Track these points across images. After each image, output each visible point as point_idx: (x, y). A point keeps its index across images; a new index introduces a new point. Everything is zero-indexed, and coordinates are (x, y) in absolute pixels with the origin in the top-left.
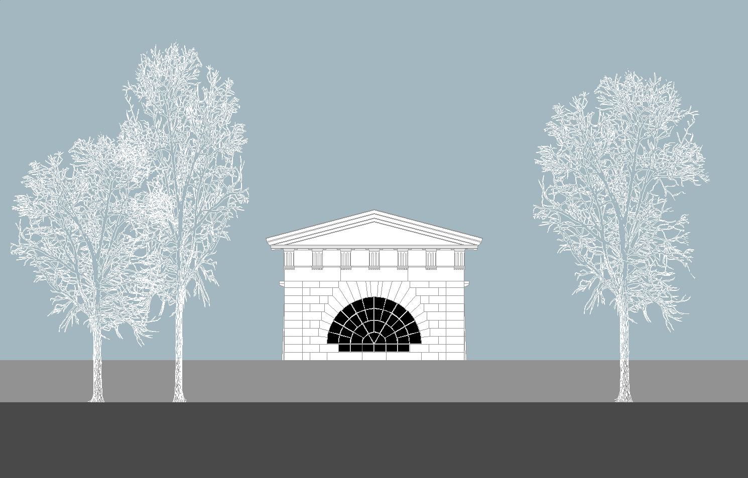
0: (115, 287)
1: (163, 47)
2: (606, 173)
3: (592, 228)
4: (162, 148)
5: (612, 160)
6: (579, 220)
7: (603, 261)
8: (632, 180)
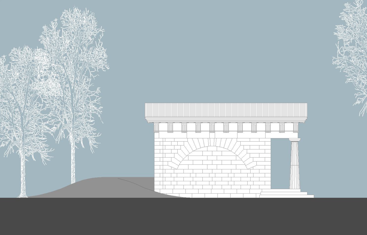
0: (32, 132)
2: (14, 92)
3: (8, 117)
5: (17, 87)
6: (357, 65)
7: (13, 133)
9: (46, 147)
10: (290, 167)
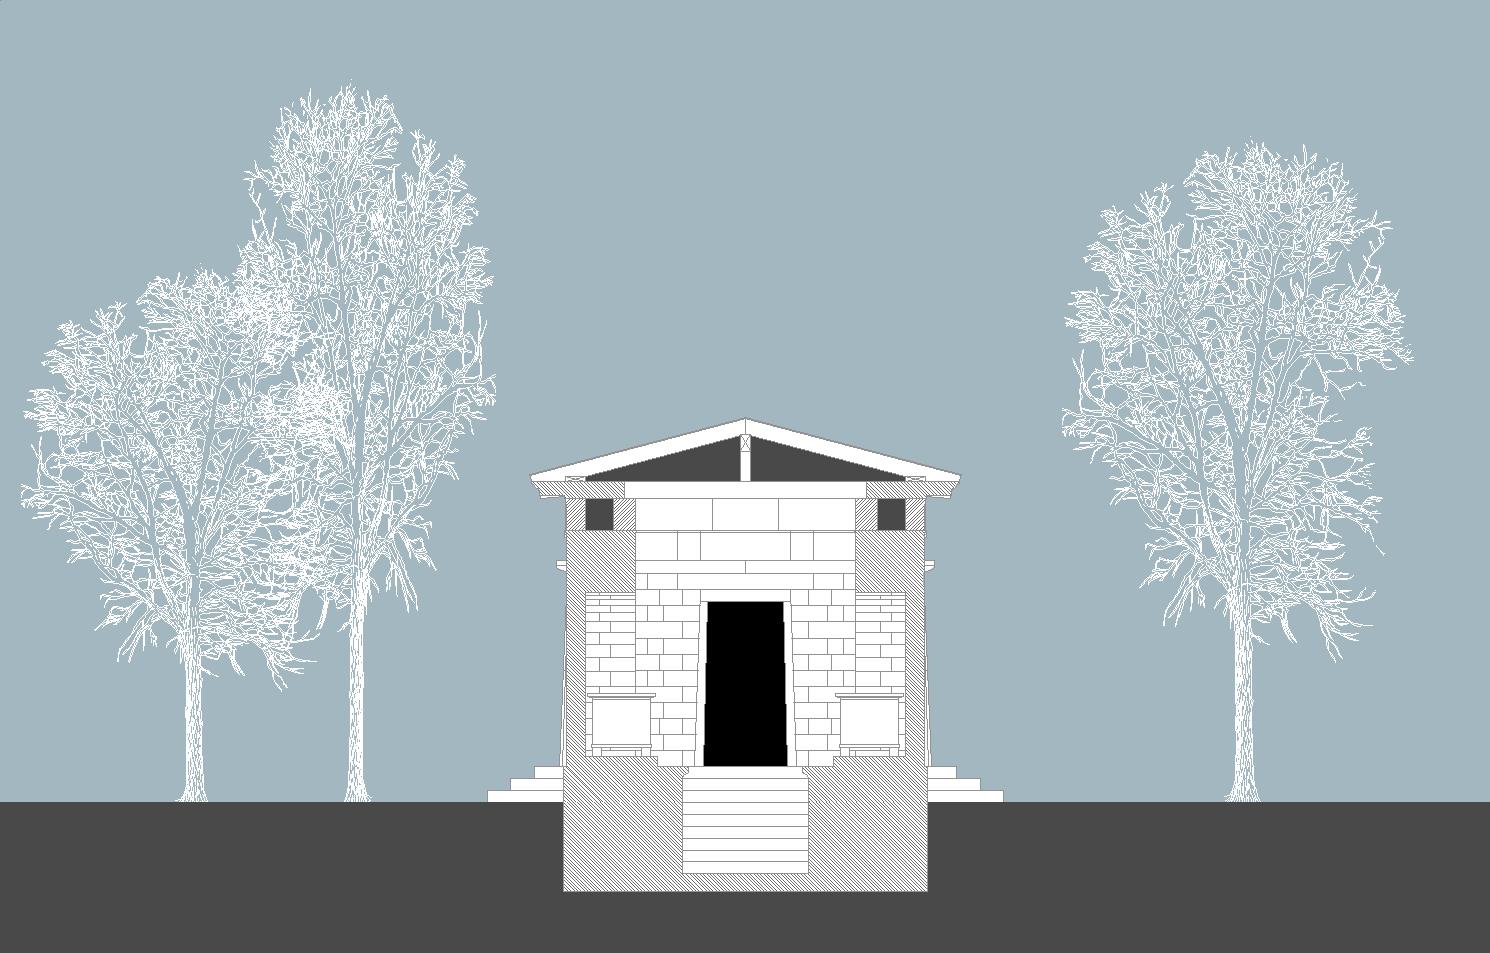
0: (228, 572)
1: (325, 95)
2: (1207, 345)
4: (323, 296)
5: (1220, 320)
6: (1153, 438)
7: (1201, 521)
8: (1259, 359)
9: (1341, 585)
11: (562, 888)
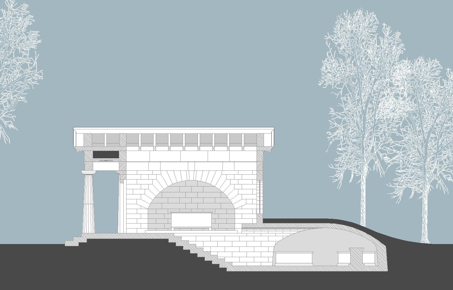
10: (83, 207)
11: (204, 260)
